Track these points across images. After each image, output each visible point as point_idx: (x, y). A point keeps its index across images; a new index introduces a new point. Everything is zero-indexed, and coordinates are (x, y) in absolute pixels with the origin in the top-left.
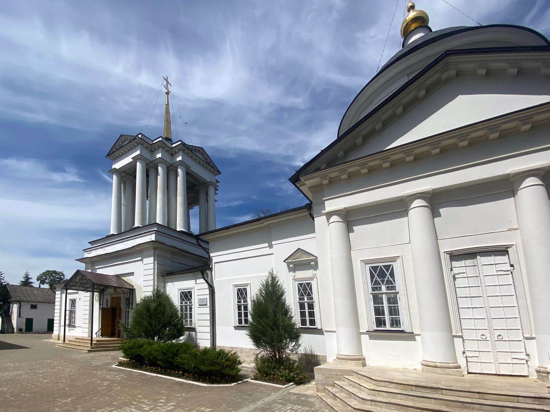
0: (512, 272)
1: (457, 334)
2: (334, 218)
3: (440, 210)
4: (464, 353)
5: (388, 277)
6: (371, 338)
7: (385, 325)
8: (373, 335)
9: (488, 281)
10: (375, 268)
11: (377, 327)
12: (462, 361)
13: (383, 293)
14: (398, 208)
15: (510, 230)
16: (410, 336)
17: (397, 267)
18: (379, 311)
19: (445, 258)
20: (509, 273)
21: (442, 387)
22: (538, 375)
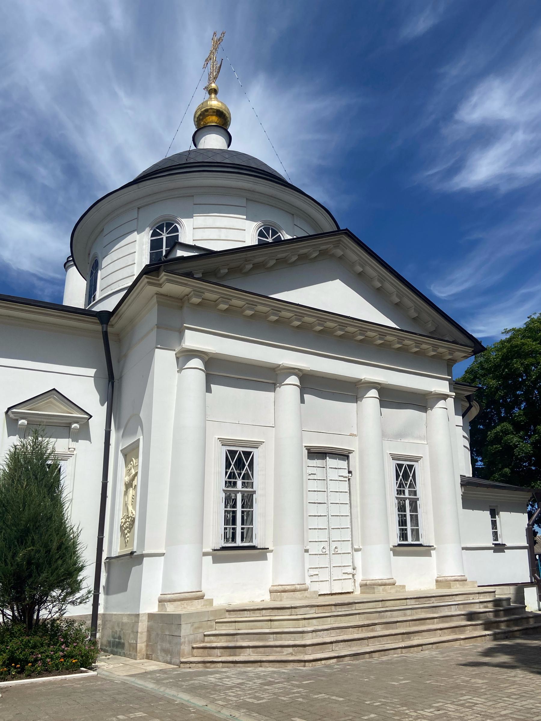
0: (349, 479)
2: (196, 363)
5: (232, 469)
6: (216, 560)
17: (257, 454)
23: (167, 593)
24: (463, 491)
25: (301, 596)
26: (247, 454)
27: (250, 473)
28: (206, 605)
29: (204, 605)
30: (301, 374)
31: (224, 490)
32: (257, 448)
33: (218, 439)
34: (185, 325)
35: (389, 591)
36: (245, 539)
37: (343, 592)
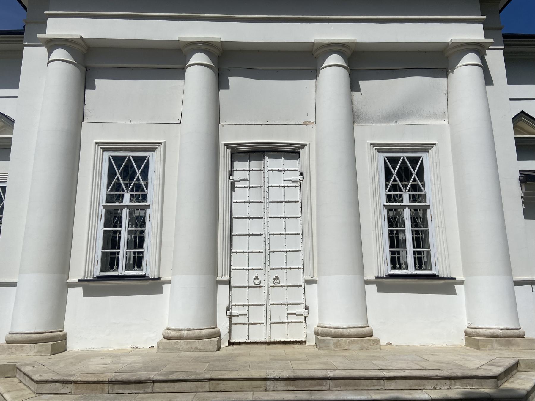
1: (223, 278)
2: (60, 53)
3: (360, 82)
4: (228, 309)
6: (381, 289)
7: (407, 268)
8: (385, 284)
9: (275, 195)
10: (393, 161)
11: (102, 270)
12: (223, 325)
13: (404, 207)
14: (302, 63)
15: (306, 123)
16: (446, 285)
17: (427, 159)
18: (111, 240)
19: (224, 154)
20: (298, 184)
21: (156, 378)
22: (317, 339)
23: (480, 327)
24: (524, 190)
25: (187, 347)
26: (414, 161)
27: (142, 182)
28: (41, 352)
29: (37, 352)
30: (349, 53)
31: (385, 206)
32: (154, 151)
33: (371, 144)
34: (45, 12)
35: (347, 347)
36: (423, 266)
37: (287, 340)
